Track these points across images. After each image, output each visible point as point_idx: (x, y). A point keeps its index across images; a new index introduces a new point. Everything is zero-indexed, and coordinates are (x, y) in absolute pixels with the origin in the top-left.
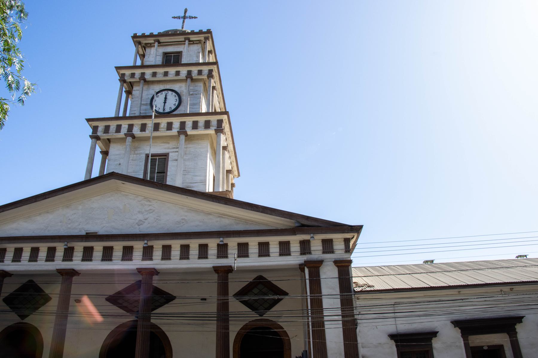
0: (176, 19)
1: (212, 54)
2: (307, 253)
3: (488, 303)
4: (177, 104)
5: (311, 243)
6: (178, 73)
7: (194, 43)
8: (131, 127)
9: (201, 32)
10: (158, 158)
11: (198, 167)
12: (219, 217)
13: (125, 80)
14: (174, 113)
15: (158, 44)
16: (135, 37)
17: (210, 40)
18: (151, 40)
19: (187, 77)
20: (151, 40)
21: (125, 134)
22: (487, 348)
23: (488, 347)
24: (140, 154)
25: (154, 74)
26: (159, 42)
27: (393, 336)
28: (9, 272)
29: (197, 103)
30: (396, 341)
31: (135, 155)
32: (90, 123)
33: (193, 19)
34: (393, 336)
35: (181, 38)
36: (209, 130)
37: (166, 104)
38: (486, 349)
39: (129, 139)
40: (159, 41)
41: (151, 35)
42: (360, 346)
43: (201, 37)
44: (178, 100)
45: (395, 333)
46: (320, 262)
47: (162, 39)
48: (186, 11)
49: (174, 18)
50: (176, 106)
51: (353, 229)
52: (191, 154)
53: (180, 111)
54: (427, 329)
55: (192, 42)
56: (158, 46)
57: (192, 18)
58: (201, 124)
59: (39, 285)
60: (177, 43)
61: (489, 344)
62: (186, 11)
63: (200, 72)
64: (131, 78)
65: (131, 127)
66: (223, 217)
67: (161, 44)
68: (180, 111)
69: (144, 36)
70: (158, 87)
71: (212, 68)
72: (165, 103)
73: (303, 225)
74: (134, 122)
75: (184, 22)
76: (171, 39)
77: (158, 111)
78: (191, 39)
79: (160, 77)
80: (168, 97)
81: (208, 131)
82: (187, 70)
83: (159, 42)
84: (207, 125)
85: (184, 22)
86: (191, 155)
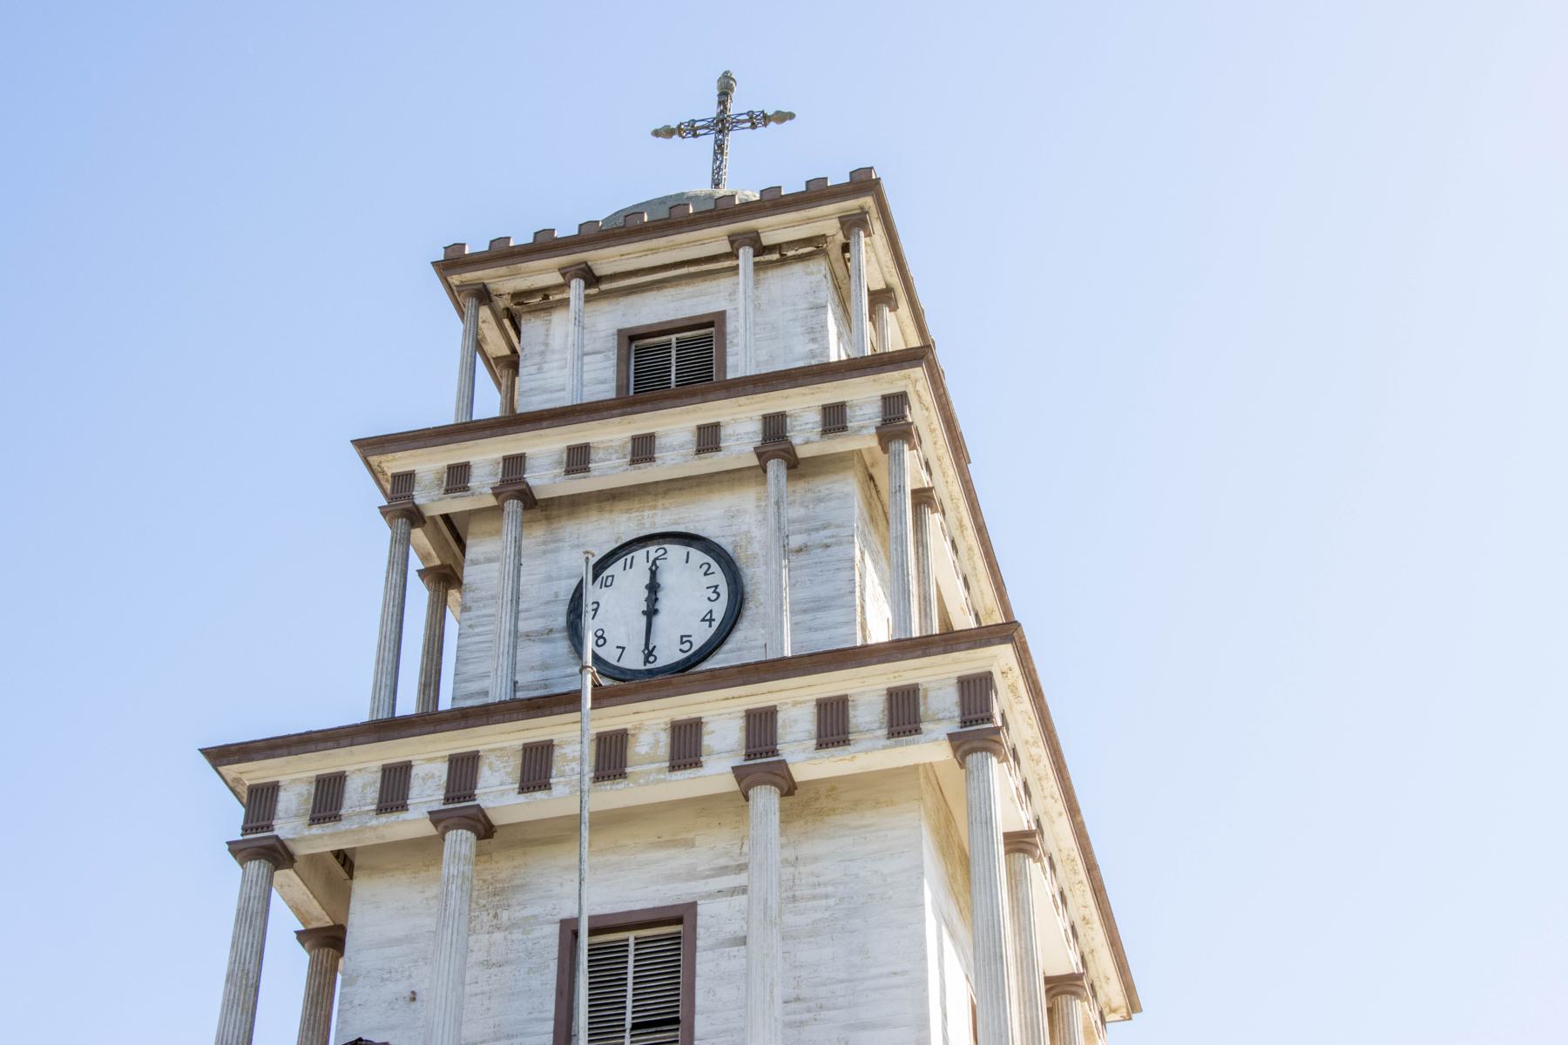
0: (676, 137)
4: (719, 616)
6: (709, 438)
7: (784, 261)
8: (464, 769)
9: (817, 193)
10: (632, 942)
15: (588, 286)
16: (452, 262)
18: (543, 273)
19: (762, 455)
20: (543, 273)
24: (526, 924)
25: (578, 459)
26: (591, 278)
29: (833, 598)
31: (498, 936)
32: (231, 770)
33: (772, 125)
35: (713, 239)
37: (658, 621)
41: (545, 245)
43: (824, 220)
44: (724, 590)
47: (606, 260)
48: (725, 89)
49: (667, 132)
50: (716, 625)
52: (827, 897)
53: (744, 647)
55: (775, 256)
57: (767, 119)
58: (868, 712)
60: (693, 269)
62: (725, 89)
63: (834, 419)
65: (464, 769)
67: (604, 287)
68: (744, 647)
69: (502, 254)
71: (903, 383)
75: (720, 148)
76: (702, 242)
77: (615, 663)
78: (768, 239)
79: (610, 471)
83: (591, 278)
85: (720, 148)
86: (823, 902)
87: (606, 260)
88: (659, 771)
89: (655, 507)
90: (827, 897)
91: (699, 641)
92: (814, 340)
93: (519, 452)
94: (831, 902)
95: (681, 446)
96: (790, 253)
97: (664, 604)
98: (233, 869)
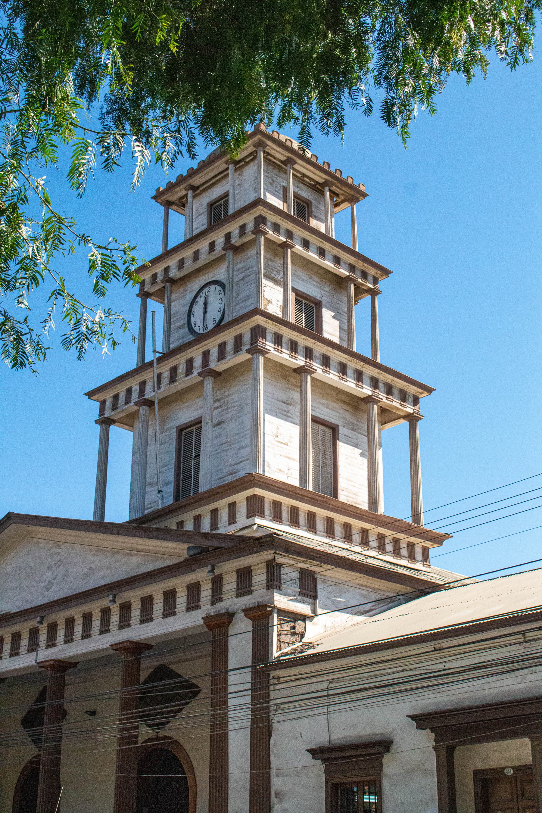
1: (295, 163)
2: (308, 595)
3: (337, 665)
5: (224, 580)
7: (247, 163)
11: (244, 429)
12: (128, 554)
13: (171, 278)
14: (223, 323)
15: (194, 191)
16: (158, 196)
17: (269, 143)
18: (180, 192)
20: (180, 192)
21: (200, 374)
22: (512, 772)
23: (514, 771)
24: (168, 430)
27: (315, 753)
28: (70, 661)
29: (250, 295)
30: (324, 760)
31: (164, 434)
32: (95, 397)
34: (315, 753)
36: (240, 354)
37: (208, 314)
38: (509, 774)
39: (209, 382)
40: (192, 186)
42: (273, 773)
45: (327, 745)
46: (230, 616)
47: (197, 181)
51: (262, 542)
52: (235, 406)
54: (378, 735)
55: (243, 163)
56: (236, 170)
59: (170, 667)
60: (222, 175)
61: (517, 764)
64: (152, 284)
66: (131, 555)
67: (201, 189)
69: (171, 187)
70: (201, 281)
71: (258, 212)
72: (205, 312)
73: (203, 550)
74: (146, 376)
76: (208, 173)
78: (238, 158)
79: (189, 266)
80: (210, 299)
81: (240, 356)
82: (223, 235)
83: (194, 188)
84: (237, 348)
86: (234, 409)
87: (197, 181)
88: (183, 377)
89: (209, 272)
90: (235, 406)
91: (217, 320)
92: (256, 192)
93: (242, 224)
94: (236, 408)
95: (205, 252)
96: (247, 160)
97: (209, 309)
98: (98, 427)
